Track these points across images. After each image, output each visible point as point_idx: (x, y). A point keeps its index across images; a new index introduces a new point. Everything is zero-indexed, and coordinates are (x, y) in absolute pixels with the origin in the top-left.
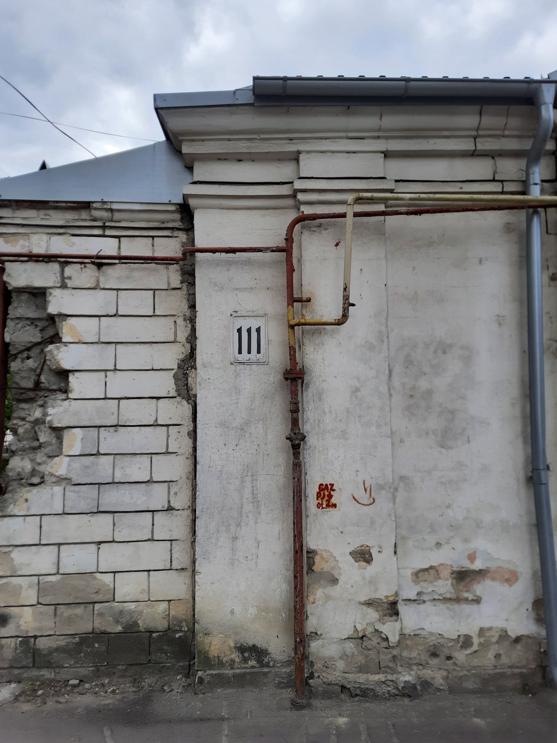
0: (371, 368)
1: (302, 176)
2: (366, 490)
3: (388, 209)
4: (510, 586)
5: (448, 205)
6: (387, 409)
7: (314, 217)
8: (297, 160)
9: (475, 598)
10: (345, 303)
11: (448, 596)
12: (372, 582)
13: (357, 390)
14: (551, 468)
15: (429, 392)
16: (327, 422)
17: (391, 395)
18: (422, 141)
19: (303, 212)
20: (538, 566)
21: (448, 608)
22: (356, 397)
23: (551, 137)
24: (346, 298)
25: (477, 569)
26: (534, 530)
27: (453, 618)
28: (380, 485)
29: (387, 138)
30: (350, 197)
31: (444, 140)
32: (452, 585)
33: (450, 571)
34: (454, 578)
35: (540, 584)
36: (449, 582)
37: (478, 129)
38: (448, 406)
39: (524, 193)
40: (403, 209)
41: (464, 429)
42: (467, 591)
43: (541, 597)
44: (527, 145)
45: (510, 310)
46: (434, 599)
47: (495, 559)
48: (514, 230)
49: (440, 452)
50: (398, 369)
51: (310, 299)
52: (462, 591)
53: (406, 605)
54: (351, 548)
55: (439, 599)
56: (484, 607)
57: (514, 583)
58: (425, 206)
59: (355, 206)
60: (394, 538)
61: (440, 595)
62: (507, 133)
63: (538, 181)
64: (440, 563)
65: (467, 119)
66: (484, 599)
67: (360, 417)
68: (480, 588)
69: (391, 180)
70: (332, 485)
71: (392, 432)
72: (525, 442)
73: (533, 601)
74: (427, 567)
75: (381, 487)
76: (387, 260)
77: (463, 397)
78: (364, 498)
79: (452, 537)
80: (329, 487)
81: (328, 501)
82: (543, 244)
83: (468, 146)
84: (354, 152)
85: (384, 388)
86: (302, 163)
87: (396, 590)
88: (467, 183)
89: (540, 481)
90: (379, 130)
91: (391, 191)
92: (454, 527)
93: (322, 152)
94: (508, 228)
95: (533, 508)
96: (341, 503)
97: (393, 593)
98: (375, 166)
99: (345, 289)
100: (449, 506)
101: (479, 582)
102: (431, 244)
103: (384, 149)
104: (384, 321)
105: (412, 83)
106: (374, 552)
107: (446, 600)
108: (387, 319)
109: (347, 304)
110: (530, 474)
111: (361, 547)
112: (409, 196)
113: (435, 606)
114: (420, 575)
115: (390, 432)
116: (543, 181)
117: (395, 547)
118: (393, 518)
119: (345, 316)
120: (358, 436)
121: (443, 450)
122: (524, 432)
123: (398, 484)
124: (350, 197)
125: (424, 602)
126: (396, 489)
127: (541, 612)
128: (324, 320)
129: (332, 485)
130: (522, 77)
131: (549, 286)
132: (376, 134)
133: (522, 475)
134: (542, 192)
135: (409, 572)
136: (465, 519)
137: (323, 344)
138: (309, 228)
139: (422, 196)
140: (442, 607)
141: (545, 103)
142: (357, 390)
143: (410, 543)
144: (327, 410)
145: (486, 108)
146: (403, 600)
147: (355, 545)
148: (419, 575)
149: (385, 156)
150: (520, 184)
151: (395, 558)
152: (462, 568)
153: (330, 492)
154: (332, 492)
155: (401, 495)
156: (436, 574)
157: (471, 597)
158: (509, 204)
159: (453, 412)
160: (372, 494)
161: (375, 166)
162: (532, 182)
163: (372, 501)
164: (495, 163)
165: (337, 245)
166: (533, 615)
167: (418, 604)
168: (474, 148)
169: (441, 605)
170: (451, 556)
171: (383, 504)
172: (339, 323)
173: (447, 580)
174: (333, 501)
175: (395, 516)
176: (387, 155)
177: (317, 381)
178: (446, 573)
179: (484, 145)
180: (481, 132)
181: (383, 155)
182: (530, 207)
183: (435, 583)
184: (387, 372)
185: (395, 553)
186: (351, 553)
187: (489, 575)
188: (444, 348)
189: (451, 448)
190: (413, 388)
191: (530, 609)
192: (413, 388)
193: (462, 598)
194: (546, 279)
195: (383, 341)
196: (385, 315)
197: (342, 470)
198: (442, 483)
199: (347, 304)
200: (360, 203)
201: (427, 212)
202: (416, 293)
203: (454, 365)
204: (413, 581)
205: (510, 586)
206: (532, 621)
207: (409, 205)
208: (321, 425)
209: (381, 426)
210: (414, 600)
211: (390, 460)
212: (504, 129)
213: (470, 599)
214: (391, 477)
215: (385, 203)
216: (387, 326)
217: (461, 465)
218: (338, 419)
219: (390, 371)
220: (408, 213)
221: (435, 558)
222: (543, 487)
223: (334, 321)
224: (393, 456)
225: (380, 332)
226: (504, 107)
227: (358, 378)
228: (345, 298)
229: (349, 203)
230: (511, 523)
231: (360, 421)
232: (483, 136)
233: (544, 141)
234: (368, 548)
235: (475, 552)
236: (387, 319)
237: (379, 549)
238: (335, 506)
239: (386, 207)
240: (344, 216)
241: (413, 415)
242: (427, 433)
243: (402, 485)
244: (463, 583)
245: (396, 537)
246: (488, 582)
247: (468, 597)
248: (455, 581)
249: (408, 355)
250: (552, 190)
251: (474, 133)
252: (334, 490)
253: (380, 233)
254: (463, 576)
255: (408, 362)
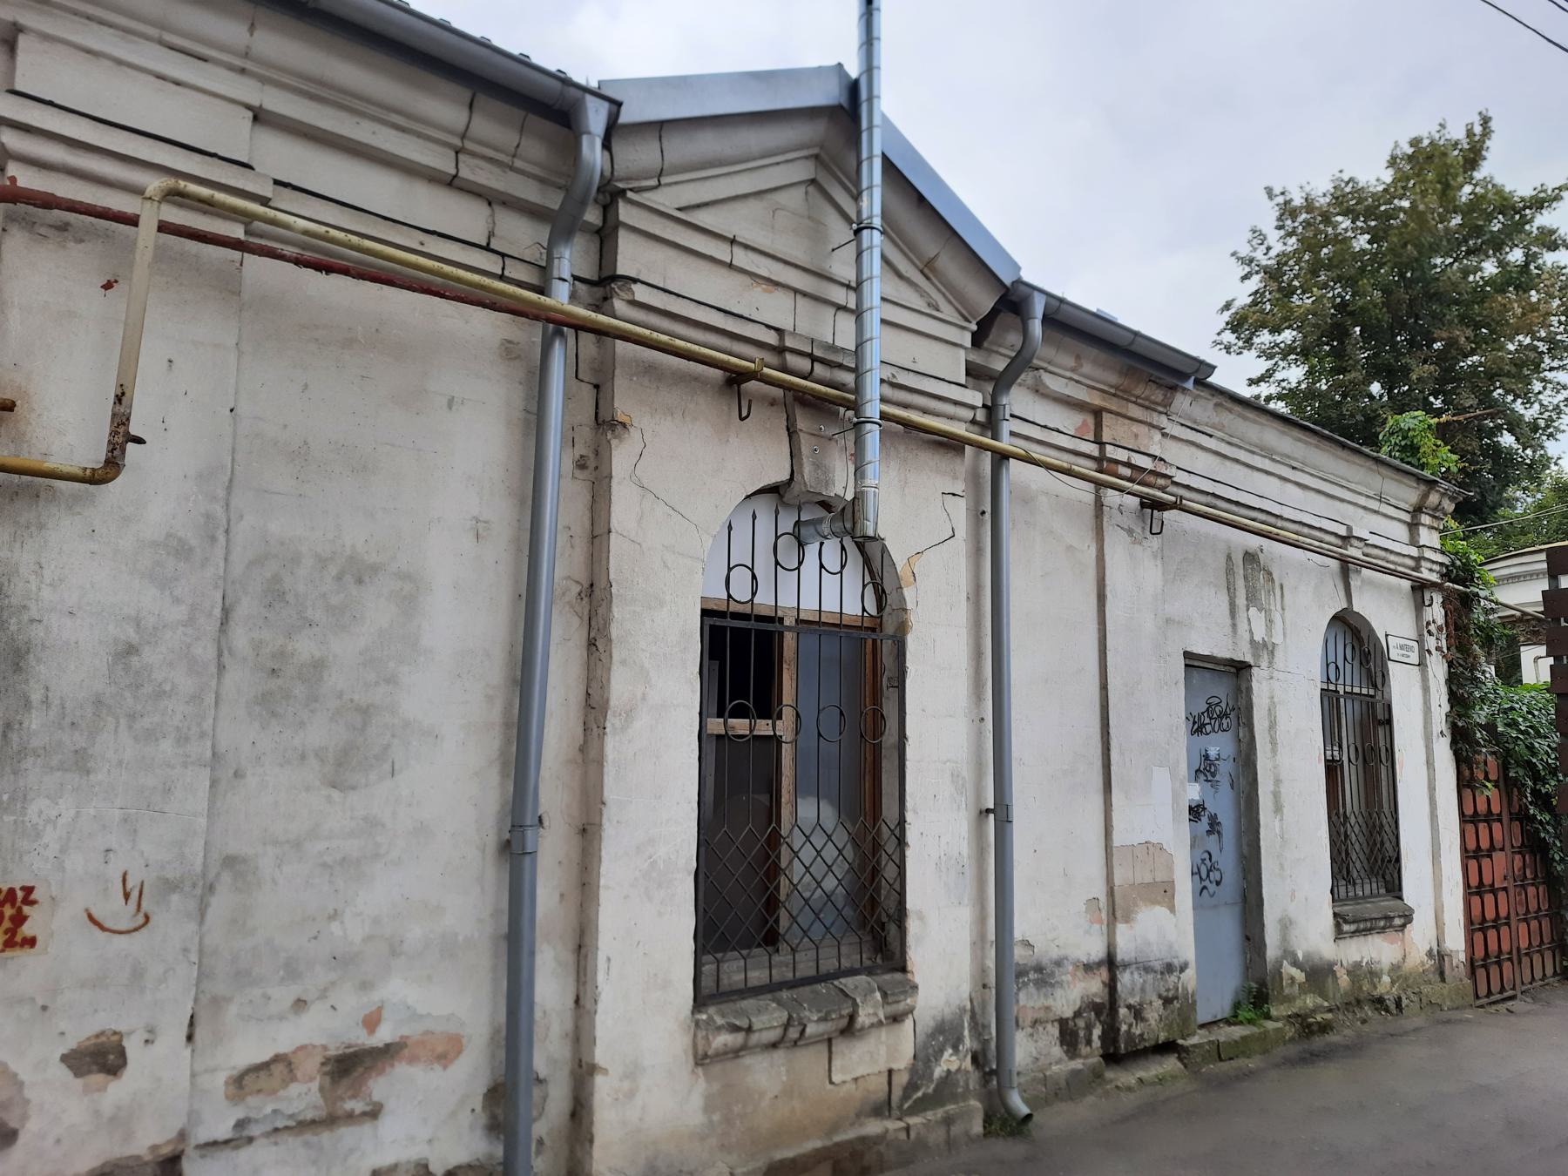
0: (177, 601)
1: (18, 87)
2: (127, 896)
3: (251, 240)
4: (445, 1068)
5: (393, 271)
6: (210, 699)
7: (48, 202)
8: (12, 48)
9: (368, 1109)
10: (117, 433)
11: (309, 1115)
12: (120, 1122)
13: (131, 650)
14: (546, 823)
15: (319, 666)
16: (34, 726)
17: (221, 668)
18: (343, 115)
19: (13, 180)
20: (502, 1018)
21: (307, 1144)
22: (127, 668)
23: (596, 201)
24: (120, 421)
25: (381, 1045)
26: (504, 946)
27: (314, 1163)
28: (167, 881)
29: (264, 80)
30: (154, 184)
31: (394, 132)
32: (321, 1089)
33: (319, 1059)
34: (326, 1074)
35: (502, 1054)
36: (315, 1086)
37: (463, 137)
38: (356, 697)
39: (541, 291)
40: (289, 250)
41: (387, 747)
42: (354, 1097)
43: (502, 1079)
44: (554, 201)
45: (502, 515)
46: (276, 1130)
47: (421, 1016)
48: (518, 357)
49: (329, 799)
50: (246, 607)
51: (13, 404)
52: (342, 1099)
53: (202, 1157)
54: (70, 1044)
55: (287, 1128)
56: (388, 1126)
57: (452, 1061)
58: (342, 257)
59: (165, 207)
60: (190, 1004)
61: (291, 1117)
62: (518, 163)
63: (567, 276)
64: (298, 1044)
65: (443, 108)
66: (390, 1105)
67: (132, 717)
68: (379, 1087)
69: (265, 176)
70: (29, 890)
71: (214, 754)
72: (504, 775)
73: (485, 1090)
74: (266, 1057)
75: (170, 886)
76: (240, 354)
77: (392, 680)
78: (115, 910)
79: (333, 983)
80: (20, 894)
81: (12, 932)
82: (567, 397)
83: (442, 161)
84: (178, 83)
85: (205, 651)
86: (21, 57)
87: (180, 1126)
88: (435, 237)
89: (524, 847)
90: (246, 55)
91: (265, 201)
92: (342, 961)
93: (89, 51)
94: (509, 351)
95: (505, 905)
96: (52, 935)
97: (172, 1134)
98: (236, 136)
99: (119, 399)
100: (334, 916)
101: (381, 1072)
102: (349, 343)
103: (255, 102)
104: (221, 493)
105: (572, 90)
106: (132, 1047)
107: (304, 1126)
108: (229, 489)
109: (122, 437)
110: (507, 836)
111: (97, 1036)
112: (302, 223)
113: (276, 1144)
114: (247, 1080)
115: (209, 753)
116: (576, 278)
117: (192, 1024)
118: (194, 958)
119: (112, 466)
120: (120, 763)
121: (336, 794)
122: (503, 753)
123: (218, 874)
124: (154, 184)
125: (250, 1140)
126: (211, 888)
127: (499, 1111)
128: (50, 464)
129: (29, 890)
130: (552, 68)
131: (573, 477)
132: (238, 62)
133: (492, 841)
134: (573, 297)
135: (221, 1078)
136: (368, 939)
137: (41, 527)
138: (30, 225)
139: (334, 233)
140: (292, 1142)
141: (589, 133)
142: (131, 650)
143: (233, 1009)
144: (36, 697)
145: (482, 100)
146: (198, 1147)
147: (78, 1034)
148: (241, 1082)
149: (256, 119)
150: (535, 270)
151: (187, 1052)
152: (349, 1047)
153: (20, 909)
154: (26, 909)
155: (221, 904)
156: (286, 1071)
157: (357, 1106)
158: (519, 307)
159: (365, 712)
160: (144, 904)
161: (236, 136)
162: (556, 274)
163: (141, 920)
164: (492, 215)
165: (108, 286)
166: (483, 1119)
167: (237, 1148)
168: (453, 172)
169: (290, 1139)
170: (329, 1026)
171: (172, 927)
172: (96, 478)
173: (312, 1079)
174: (27, 930)
175: (201, 952)
176: (259, 117)
177: (13, 621)
178: (310, 1065)
179: (472, 171)
180: (469, 145)
181: (250, 114)
182: (549, 320)
183: (282, 1093)
184: (217, 612)
185: (190, 1038)
186: (65, 1059)
187: (406, 1052)
188: (359, 572)
189: (353, 788)
190: (281, 654)
191: (479, 1108)
192: (281, 654)
193: (340, 1113)
194: (568, 465)
195: (213, 539)
196: (226, 479)
197: (63, 850)
198: (325, 865)
199: (122, 437)
200: (175, 203)
201: (345, 272)
202: (306, 443)
203: (378, 612)
204: (227, 1097)
205: (445, 1068)
206: (479, 1132)
207: (304, 247)
208: (14, 737)
209: (187, 739)
210: (227, 1142)
211: (203, 821)
212: (514, 156)
213: (357, 1112)
214: (199, 860)
215: (246, 225)
216: (227, 505)
217: (372, 824)
218: (68, 720)
219: (226, 612)
220: (298, 262)
221: (286, 1038)
222: (527, 859)
223: (80, 473)
224: (212, 813)
225: (208, 516)
226: (518, 114)
227: (137, 623)
228: (117, 420)
229: (147, 194)
230: (460, 938)
231: (130, 727)
232: (473, 154)
233: (583, 204)
234: (115, 1038)
235: (380, 1009)
236: (229, 489)
237: (146, 1036)
238: (31, 942)
239: (246, 233)
240: (133, 221)
241: (274, 714)
242: (303, 757)
243: (226, 877)
244: (345, 1082)
245: (196, 1000)
246: (401, 1070)
247: (353, 1110)
248: (328, 1079)
249: (276, 579)
250: (590, 301)
251: (457, 142)
252: (33, 903)
253: (229, 287)
254: (348, 1067)
255: (275, 594)
